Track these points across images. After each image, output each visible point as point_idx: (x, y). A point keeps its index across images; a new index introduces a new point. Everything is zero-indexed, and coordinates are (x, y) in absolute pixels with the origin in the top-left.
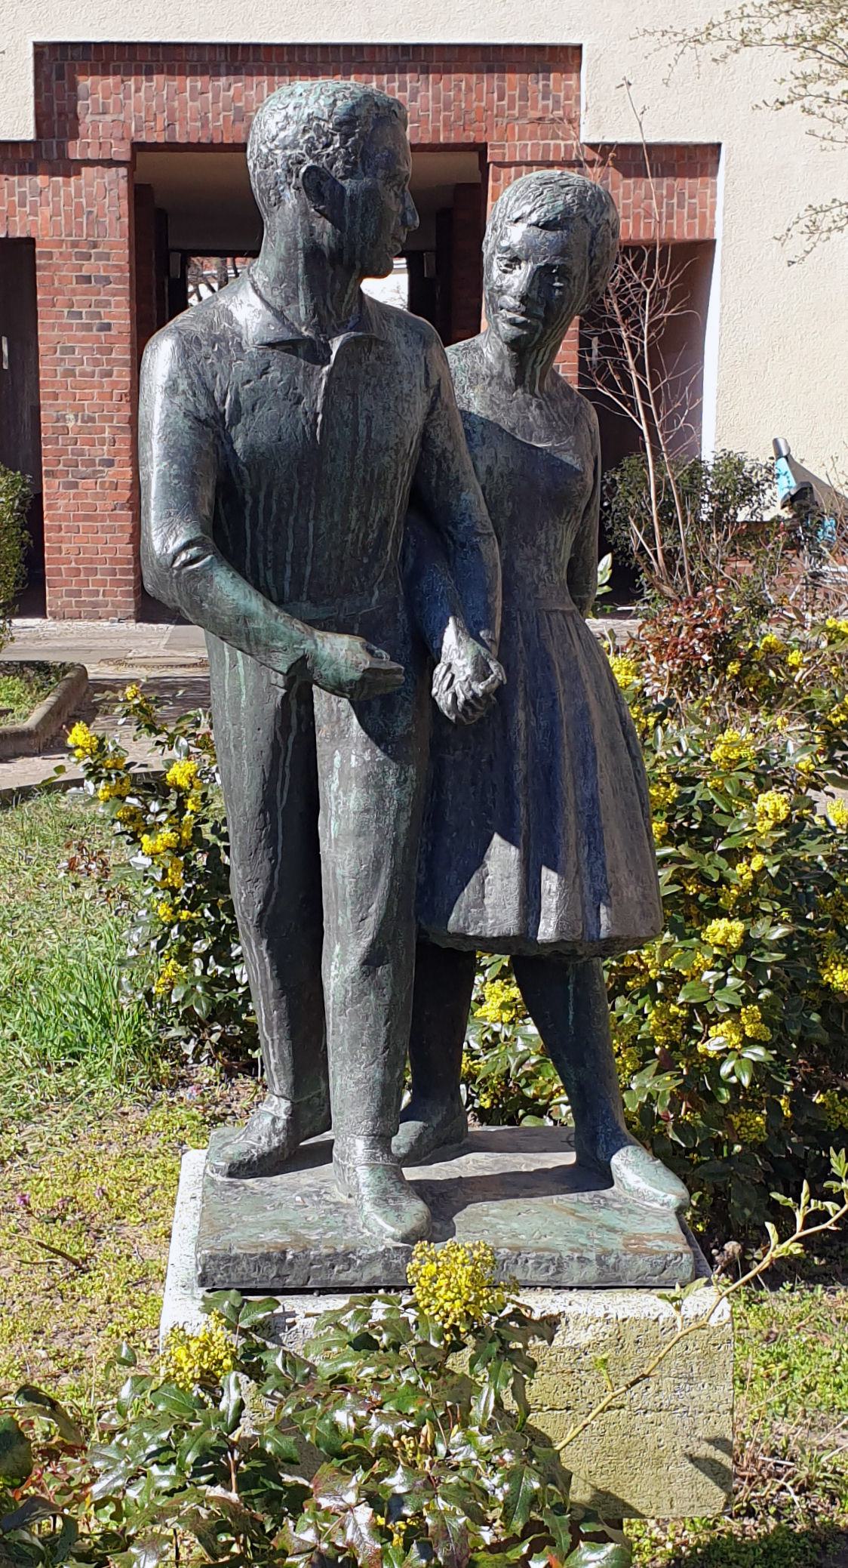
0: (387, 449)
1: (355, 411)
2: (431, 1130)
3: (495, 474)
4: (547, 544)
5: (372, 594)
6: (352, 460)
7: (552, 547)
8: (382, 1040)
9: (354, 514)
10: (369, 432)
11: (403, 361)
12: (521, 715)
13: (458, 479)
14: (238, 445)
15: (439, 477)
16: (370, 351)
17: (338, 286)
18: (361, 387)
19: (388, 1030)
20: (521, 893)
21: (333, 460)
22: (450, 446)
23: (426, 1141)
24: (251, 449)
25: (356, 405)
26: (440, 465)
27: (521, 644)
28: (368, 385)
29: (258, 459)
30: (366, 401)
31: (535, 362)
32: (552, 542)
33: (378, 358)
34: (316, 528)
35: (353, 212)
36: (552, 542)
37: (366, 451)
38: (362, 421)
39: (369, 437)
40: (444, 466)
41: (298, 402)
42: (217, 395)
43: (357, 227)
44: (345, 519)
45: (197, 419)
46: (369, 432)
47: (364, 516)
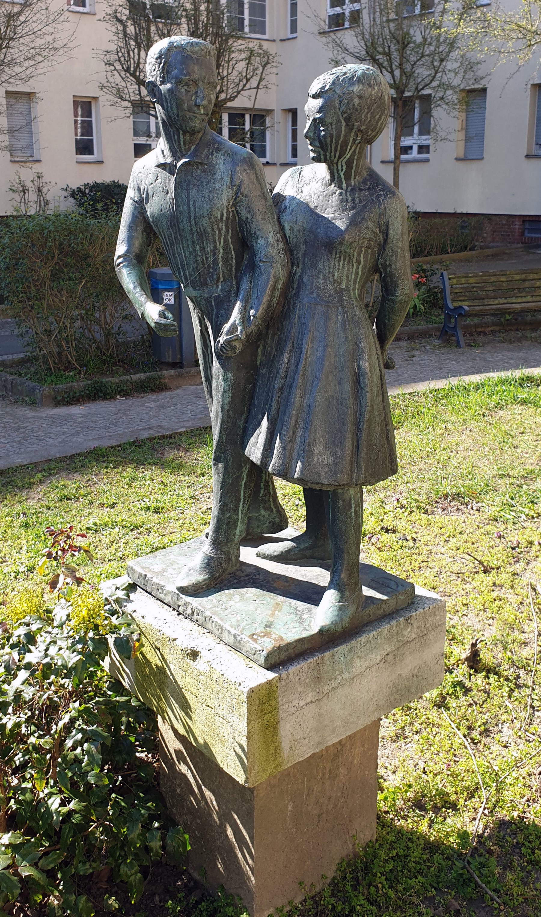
0: (204, 217)
1: (188, 198)
2: (298, 549)
3: (295, 230)
4: (324, 269)
5: (217, 287)
6: (190, 222)
7: (327, 271)
8: (219, 497)
9: (198, 248)
10: (195, 208)
11: (219, 173)
12: (286, 357)
13: (255, 233)
14: (148, 213)
15: (247, 231)
16: (198, 168)
17: (176, 137)
18: (191, 186)
19: (221, 494)
20: (265, 444)
21: (182, 221)
22: (249, 216)
23: (292, 553)
24: (152, 216)
25: (188, 195)
26: (246, 225)
27: (296, 320)
28: (195, 185)
29: (158, 219)
30: (193, 193)
31: (338, 170)
32: (327, 268)
33: (203, 171)
34: (185, 254)
35: (166, 101)
36: (327, 268)
37: (195, 218)
38: (191, 203)
39: (195, 211)
40: (248, 226)
41: (167, 193)
42: (142, 190)
43: (169, 108)
44: (195, 250)
45: (134, 200)
46: (195, 208)
47: (203, 249)
